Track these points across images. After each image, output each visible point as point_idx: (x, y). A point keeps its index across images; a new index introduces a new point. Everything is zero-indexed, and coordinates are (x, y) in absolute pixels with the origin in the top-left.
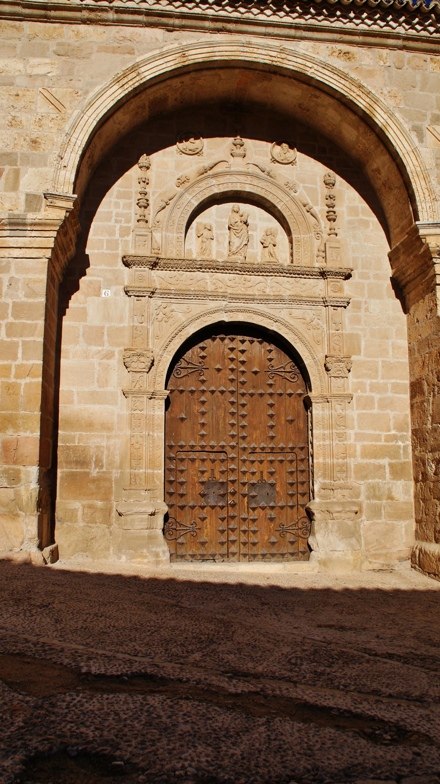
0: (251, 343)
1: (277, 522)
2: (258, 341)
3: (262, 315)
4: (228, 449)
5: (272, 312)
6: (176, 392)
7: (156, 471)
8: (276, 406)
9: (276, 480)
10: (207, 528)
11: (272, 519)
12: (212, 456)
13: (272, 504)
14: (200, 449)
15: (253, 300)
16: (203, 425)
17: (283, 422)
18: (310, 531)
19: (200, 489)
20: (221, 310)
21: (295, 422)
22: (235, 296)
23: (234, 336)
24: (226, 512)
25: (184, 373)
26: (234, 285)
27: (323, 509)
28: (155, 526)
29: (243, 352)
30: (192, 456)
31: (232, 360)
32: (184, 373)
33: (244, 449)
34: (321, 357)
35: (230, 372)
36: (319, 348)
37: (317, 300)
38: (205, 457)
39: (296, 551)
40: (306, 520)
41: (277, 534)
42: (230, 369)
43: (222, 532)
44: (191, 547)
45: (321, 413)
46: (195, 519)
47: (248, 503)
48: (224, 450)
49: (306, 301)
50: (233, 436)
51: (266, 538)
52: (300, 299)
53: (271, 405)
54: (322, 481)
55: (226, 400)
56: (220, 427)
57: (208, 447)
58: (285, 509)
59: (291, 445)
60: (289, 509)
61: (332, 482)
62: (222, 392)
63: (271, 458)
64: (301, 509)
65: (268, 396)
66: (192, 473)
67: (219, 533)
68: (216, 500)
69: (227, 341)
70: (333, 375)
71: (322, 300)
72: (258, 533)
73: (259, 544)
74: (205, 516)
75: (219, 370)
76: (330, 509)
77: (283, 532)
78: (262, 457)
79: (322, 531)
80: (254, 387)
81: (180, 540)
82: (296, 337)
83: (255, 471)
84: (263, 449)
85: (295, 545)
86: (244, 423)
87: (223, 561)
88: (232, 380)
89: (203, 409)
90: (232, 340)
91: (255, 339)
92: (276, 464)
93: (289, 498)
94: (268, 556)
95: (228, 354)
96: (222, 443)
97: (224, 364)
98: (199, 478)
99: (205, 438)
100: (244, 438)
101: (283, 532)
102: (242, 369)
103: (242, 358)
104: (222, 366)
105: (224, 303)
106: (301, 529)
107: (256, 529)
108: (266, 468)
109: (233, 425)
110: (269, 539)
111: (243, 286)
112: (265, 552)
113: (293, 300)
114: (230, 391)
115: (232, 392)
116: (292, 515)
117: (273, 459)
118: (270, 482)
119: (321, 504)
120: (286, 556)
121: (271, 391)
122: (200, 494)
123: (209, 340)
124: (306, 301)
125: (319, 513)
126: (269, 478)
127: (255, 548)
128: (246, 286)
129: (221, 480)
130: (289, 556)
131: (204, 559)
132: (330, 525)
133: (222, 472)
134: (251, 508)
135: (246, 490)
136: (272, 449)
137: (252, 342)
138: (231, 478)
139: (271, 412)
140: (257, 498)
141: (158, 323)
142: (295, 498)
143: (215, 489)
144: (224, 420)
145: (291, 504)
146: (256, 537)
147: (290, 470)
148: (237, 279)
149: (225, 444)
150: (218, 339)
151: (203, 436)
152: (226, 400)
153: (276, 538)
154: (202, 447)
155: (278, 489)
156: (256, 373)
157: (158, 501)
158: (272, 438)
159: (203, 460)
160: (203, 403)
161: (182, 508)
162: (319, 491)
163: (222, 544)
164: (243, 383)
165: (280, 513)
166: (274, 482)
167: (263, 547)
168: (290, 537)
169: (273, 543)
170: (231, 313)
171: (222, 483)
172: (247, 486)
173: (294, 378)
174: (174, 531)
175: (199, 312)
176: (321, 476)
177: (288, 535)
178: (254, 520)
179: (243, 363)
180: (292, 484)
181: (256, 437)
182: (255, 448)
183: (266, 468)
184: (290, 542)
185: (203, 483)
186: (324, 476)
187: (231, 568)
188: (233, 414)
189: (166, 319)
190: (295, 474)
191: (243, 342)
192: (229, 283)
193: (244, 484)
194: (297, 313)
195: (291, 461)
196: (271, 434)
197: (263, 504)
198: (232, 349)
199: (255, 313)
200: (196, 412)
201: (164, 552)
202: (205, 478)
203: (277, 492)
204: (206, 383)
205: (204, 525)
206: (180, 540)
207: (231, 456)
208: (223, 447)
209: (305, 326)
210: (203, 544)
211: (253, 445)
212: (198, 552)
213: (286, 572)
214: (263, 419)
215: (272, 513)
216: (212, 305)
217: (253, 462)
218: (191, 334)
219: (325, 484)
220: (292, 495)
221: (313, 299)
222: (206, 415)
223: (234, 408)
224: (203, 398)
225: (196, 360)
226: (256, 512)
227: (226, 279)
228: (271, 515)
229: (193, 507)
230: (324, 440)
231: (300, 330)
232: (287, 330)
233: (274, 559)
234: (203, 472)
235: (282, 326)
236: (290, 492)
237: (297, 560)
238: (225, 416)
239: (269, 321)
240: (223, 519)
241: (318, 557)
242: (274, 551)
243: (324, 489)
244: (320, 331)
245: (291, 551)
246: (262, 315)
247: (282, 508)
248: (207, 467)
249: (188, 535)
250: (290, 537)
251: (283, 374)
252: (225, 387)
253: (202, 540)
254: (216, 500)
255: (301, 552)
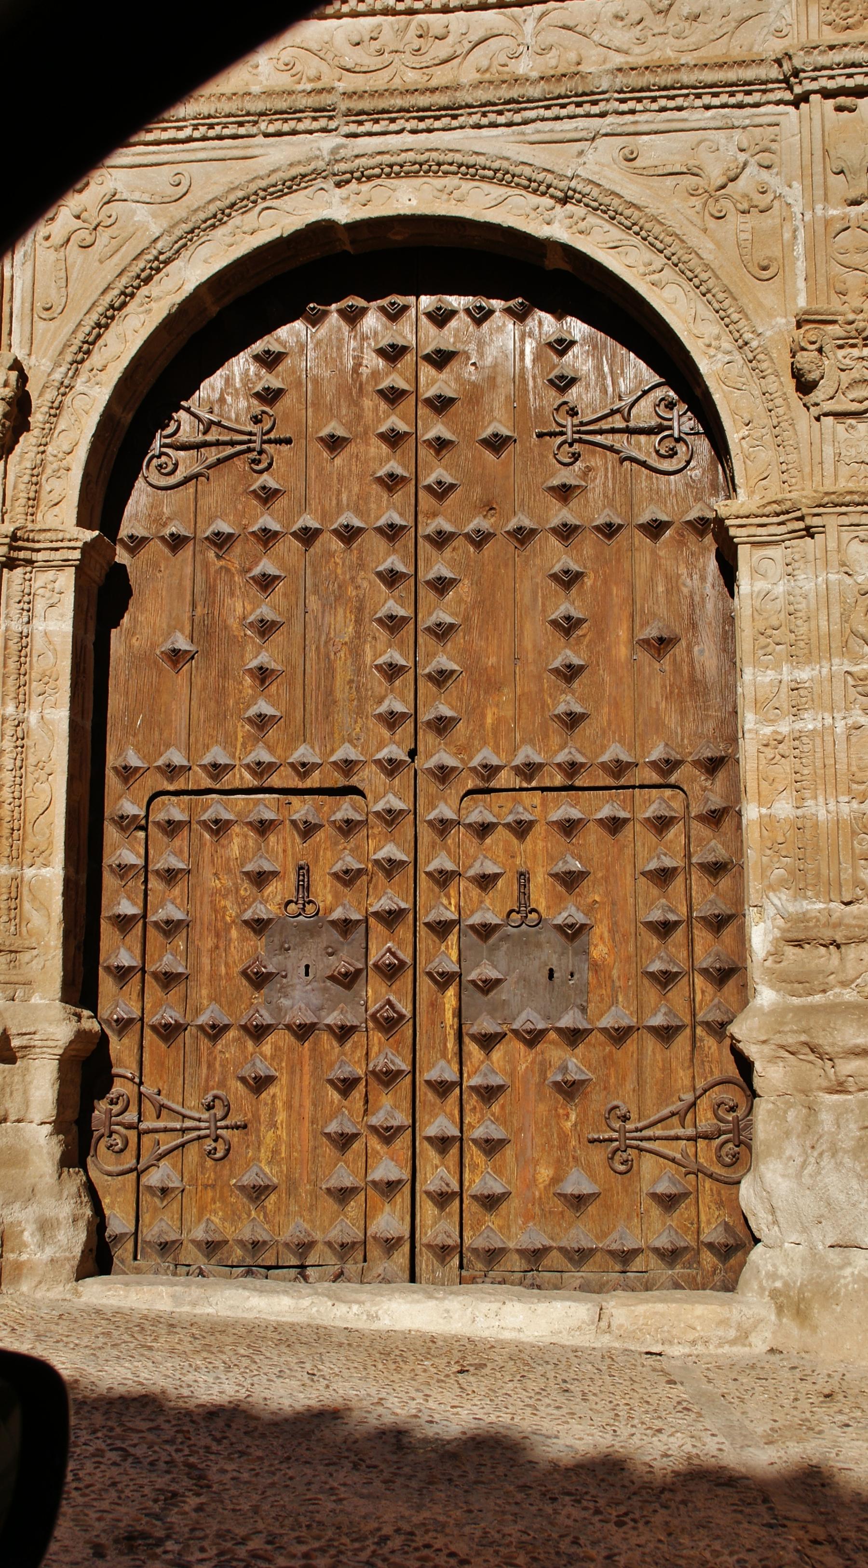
0: (479, 322)
1: (597, 1101)
2: (508, 311)
3: (501, 176)
4: (369, 777)
5: (541, 157)
6: (157, 546)
7: (29, 872)
8: (588, 582)
9: (590, 909)
10: (273, 1125)
11: (570, 1090)
12: (302, 809)
13: (567, 1021)
14: (250, 780)
15: (452, 110)
16: (263, 675)
17: (622, 652)
18: (738, 1148)
19: (242, 949)
20: (317, 173)
21: (679, 650)
22: (366, 104)
23: (401, 300)
24: (360, 1053)
25: (187, 463)
26: (373, 62)
27: (791, 1040)
28: (13, 1110)
29: (441, 359)
30: (216, 808)
31: (393, 396)
32: (187, 463)
33: (443, 774)
34: (775, 328)
35: (385, 448)
36: (767, 295)
37: (749, 74)
38: (269, 815)
39: (689, 1240)
40: (731, 1095)
41: (598, 1155)
42: (382, 436)
43: (344, 1141)
44: (202, 1210)
45: (780, 589)
46: (222, 1084)
47: (459, 1013)
48: (354, 781)
49: (698, 89)
50: (392, 720)
51: (545, 1173)
52: (667, 79)
53: (568, 580)
54: (792, 908)
55: (361, 566)
56: (339, 682)
57: (286, 771)
58: (631, 1045)
59: (657, 753)
60: (651, 1043)
61: (836, 906)
62: (349, 535)
63: (565, 809)
64: (709, 1043)
65: (554, 541)
66: (208, 889)
67: (328, 1150)
68: (316, 1000)
69: (372, 321)
70: (827, 407)
71: (774, 73)
72: (509, 1151)
73: (514, 1204)
74: (263, 1069)
75: (334, 444)
76: (824, 1041)
77: (623, 1150)
78: (529, 805)
79: (792, 1148)
80: (489, 508)
81: (154, 1178)
82: (659, 261)
83: (491, 868)
84: (529, 770)
85: (684, 1210)
86: (443, 660)
87: (338, 1277)
88: (392, 483)
89: (266, 611)
90: (394, 315)
91: (497, 304)
92: (593, 835)
93: (651, 993)
94: (555, 1259)
95: (375, 375)
96: (345, 752)
97: (359, 417)
98: (243, 903)
99: (272, 733)
100: (442, 726)
101: (623, 1150)
102: (438, 429)
103: (434, 382)
104: (348, 426)
105: (327, 143)
106: (707, 1137)
107: (497, 1132)
108: (541, 856)
109: (392, 672)
110: (556, 1180)
111: (409, 59)
112: (540, 1240)
113: (638, 93)
114: (379, 530)
115: (392, 533)
116: (667, 1069)
117: (575, 814)
118: (559, 920)
119: (779, 1014)
120: (638, 1263)
121: (561, 514)
122: (244, 973)
123: (298, 325)
124: (698, 89)
125: (774, 1060)
126: (557, 902)
127: (492, 1221)
128: (426, 60)
129: (338, 914)
130: (654, 1261)
131: (258, 1262)
132: (826, 1118)
133: (347, 878)
134: (473, 1037)
135: (447, 956)
136: (572, 768)
137: (480, 317)
138: (383, 903)
139: (564, 607)
140: (502, 994)
141: (52, 255)
142: (678, 994)
143: (310, 953)
144: (356, 653)
145: (658, 1020)
146: (499, 1171)
147: (653, 865)
148: (387, 37)
149: (353, 754)
150: (334, 318)
151: (262, 722)
152: (361, 566)
153: (593, 1177)
154: (261, 769)
155: (599, 951)
156: (497, 444)
157: (36, 1000)
158: (572, 721)
159: (263, 828)
160: (266, 583)
161: (169, 1032)
162: (776, 954)
163: (343, 1195)
164: (442, 491)
165: (608, 1061)
166: (580, 918)
167: (528, 1217)
168: (655, 1175)
169: (579, 1201)
170: (365, 187)
171: (346, 926)
172: (453, 938)
173: (672, 454)
174: (132, 1135)
175: (217, 190)
176: (782, 883)
177: (648, 1164)
178: (489, 1093)
179: (441, 405)
180: (664, 929)
181: (499, 721)
182: (492, 771)
183: (541, 856)
184: (658, 1198)
185: (259, 926)
186: (799, 881)
187: (341, 1310)
188: (393, 624)
189: (84, 235)
190: (679, 882)
191: (440, 318)
192: (351, 57)
193: (442, 929)
194: (656, 150)
195: (661, 824)
196: (568, 702)
197: (529, 1018)
198: (393, 354)
199: (470, 171)
200: (233, 623)
201: (45, 1227)
202: (269, 904)
203: (596, 967)
204: (280, 503)
205: (264, 1112)
206: (154, 1178)
207: (379, 807)
208: (348, 766)
209: (697, 202)
210: (258, 1193)
211: (486, 755)
212: (230, 1232)
213: (606, 1341)
214: (528, 644)
215: (573, 1063)
216: (276, 155)
217: (484, 830)
218: (189, 288)
219: (804, 918)
220: (665, 980)
221: (731, 75)
222: (278, 637)
223: (400, 601)
224: (266, 566)
225: (239, 409)
226: (497, 1054)
227: (340, 40)
228: (564, 1069)
229: (216, 1032)
230: (797, 711)
231: (675, 223)
232: (616, 234)
233: (576, 1277)
234: (260, 879)
235: (592, 220)
236: (656, 966)
237: (694, 1285)
238: (358, 635)
239: (535, 200)
240: (346, 1086)
241: (773, 1276)
242: (579, 1234)
243: (798, 943)
244: (769, 221)
245: (663, 1241)
246: (501, 176)
247: (619, 1036)
248: (281, 852)
249: (193, 1152)
250: (655, 1175)
251: (619, 441)
252: (358, 512)
253: (249, 1178)
254: (316, 1000)
255: (710, 1246)
